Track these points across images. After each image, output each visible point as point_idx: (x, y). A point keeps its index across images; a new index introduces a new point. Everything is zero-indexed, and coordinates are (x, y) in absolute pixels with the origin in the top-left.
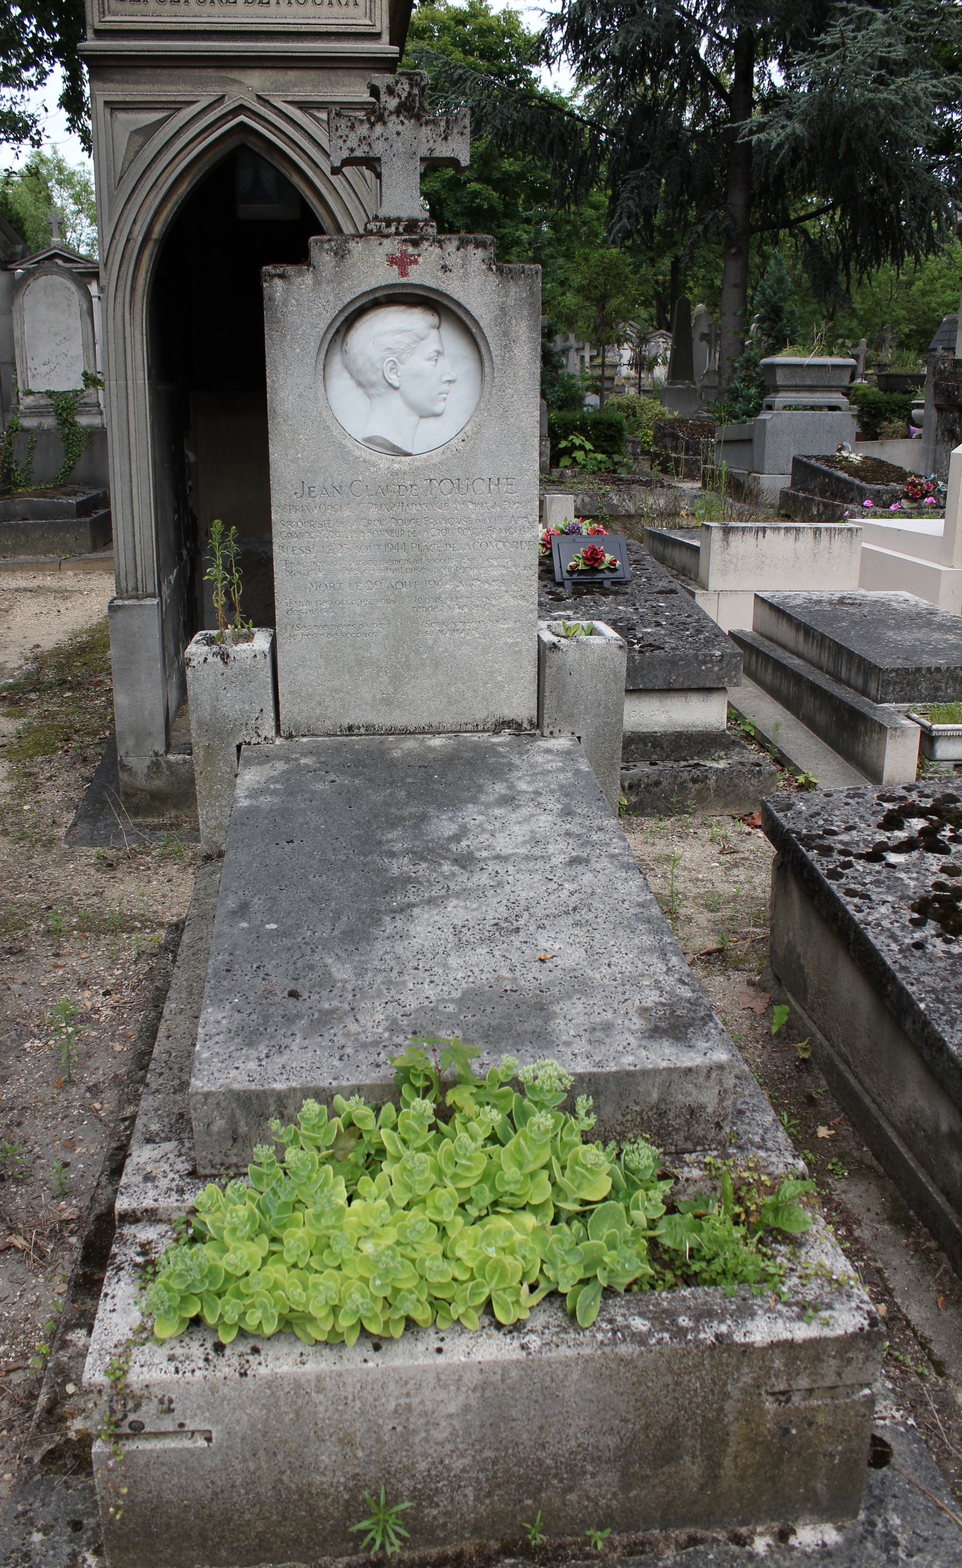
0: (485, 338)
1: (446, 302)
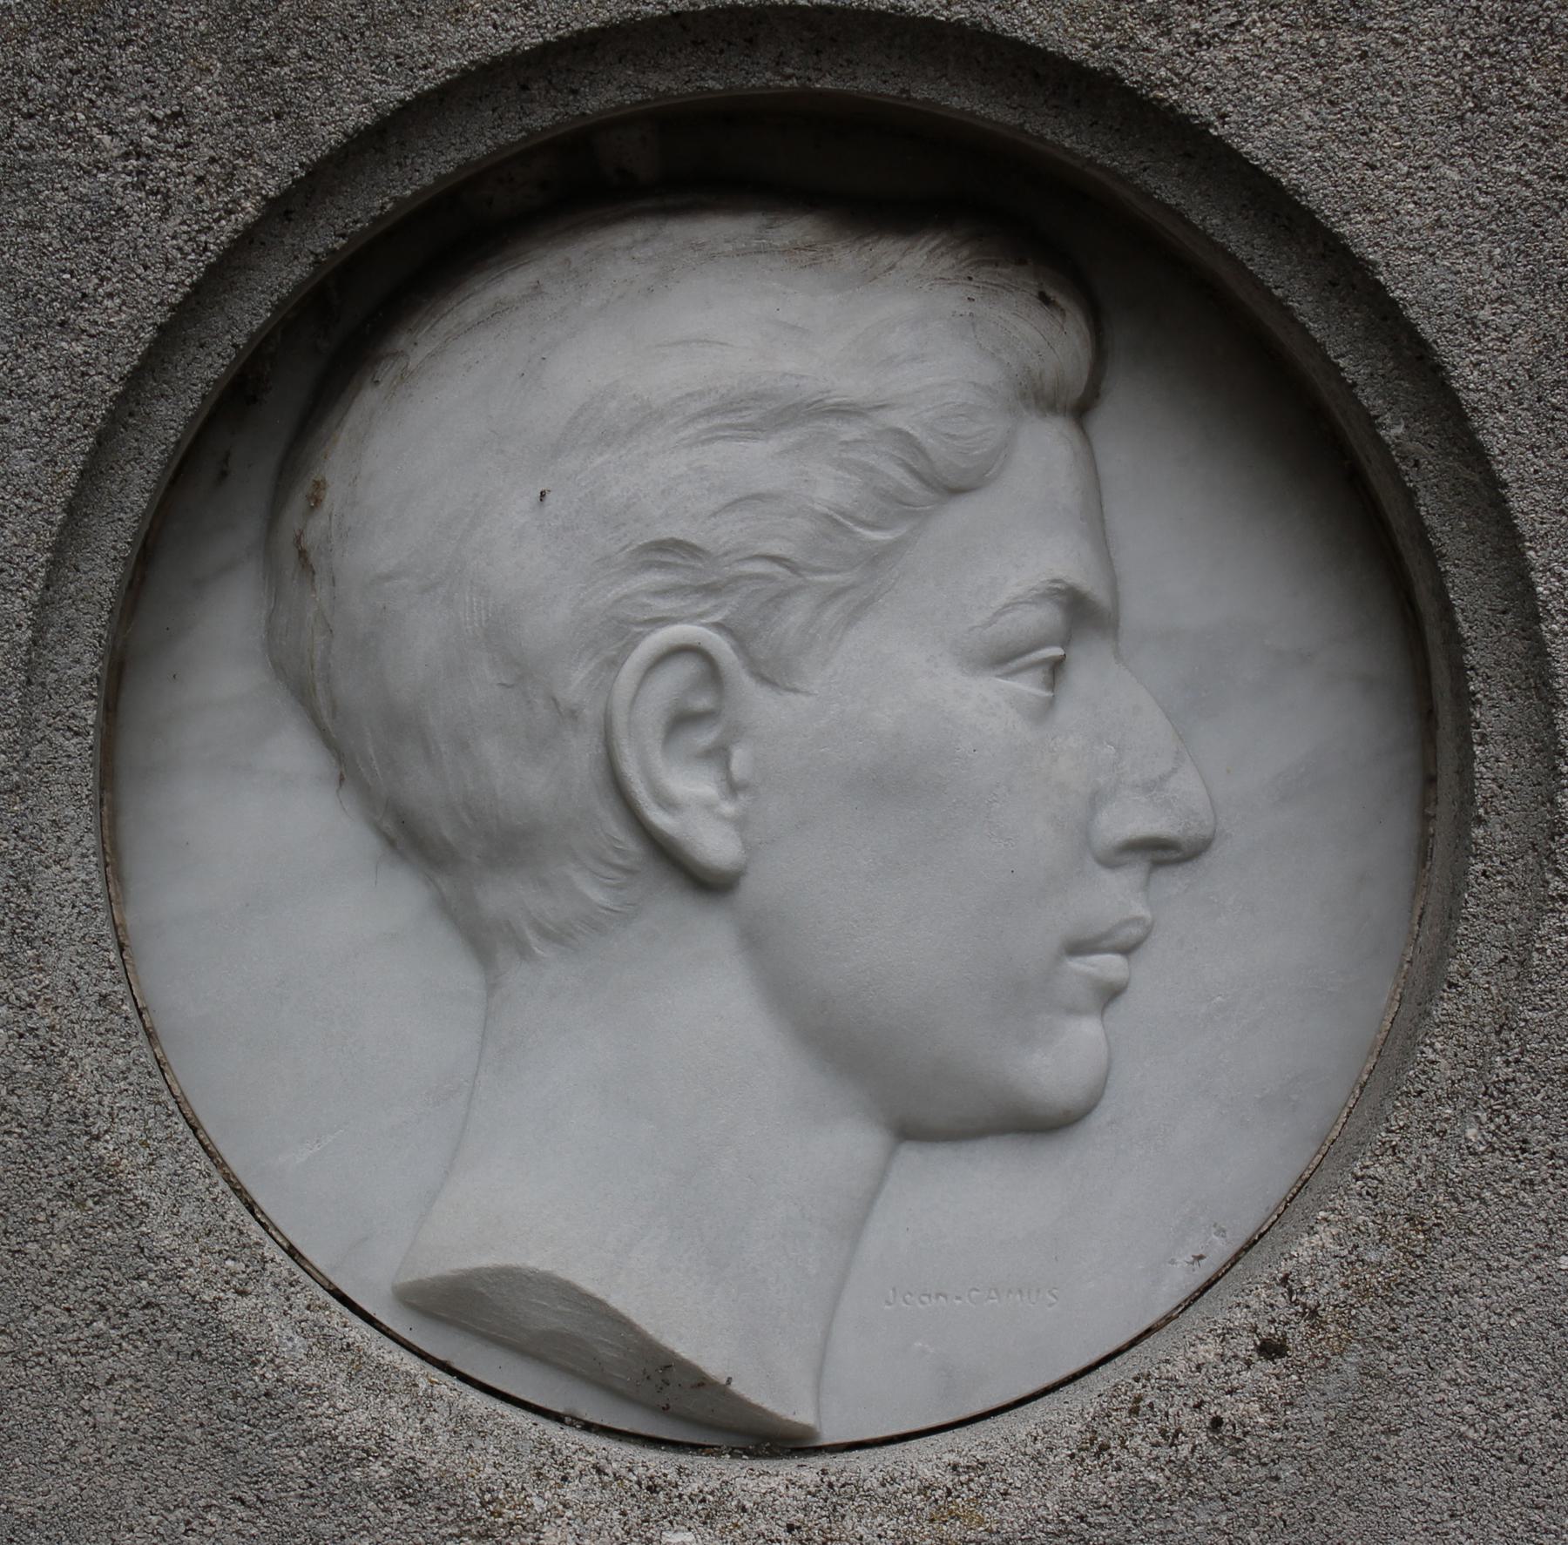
0: (1487, 496)
1: (1169, 188)
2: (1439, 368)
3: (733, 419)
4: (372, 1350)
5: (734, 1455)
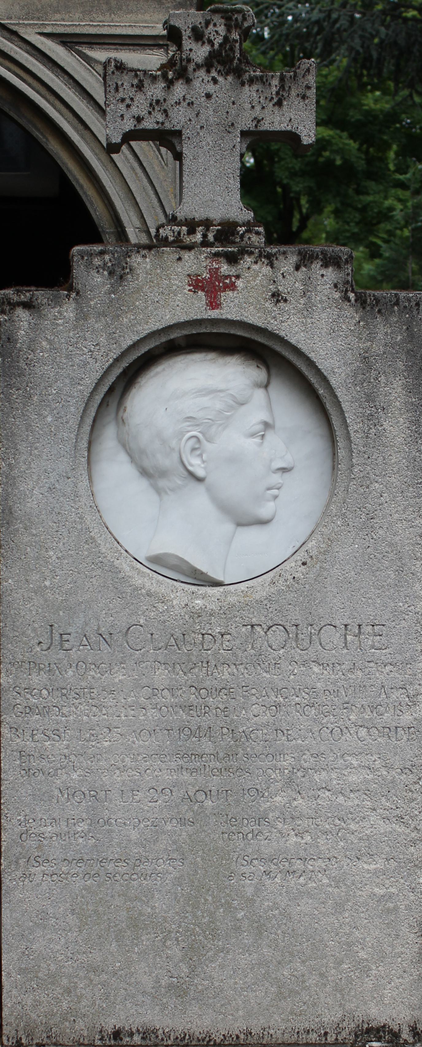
1: (278, 348)
2: (328, 381)
3: (200, 393)
4: (141, 569)
5: (209, 586)
